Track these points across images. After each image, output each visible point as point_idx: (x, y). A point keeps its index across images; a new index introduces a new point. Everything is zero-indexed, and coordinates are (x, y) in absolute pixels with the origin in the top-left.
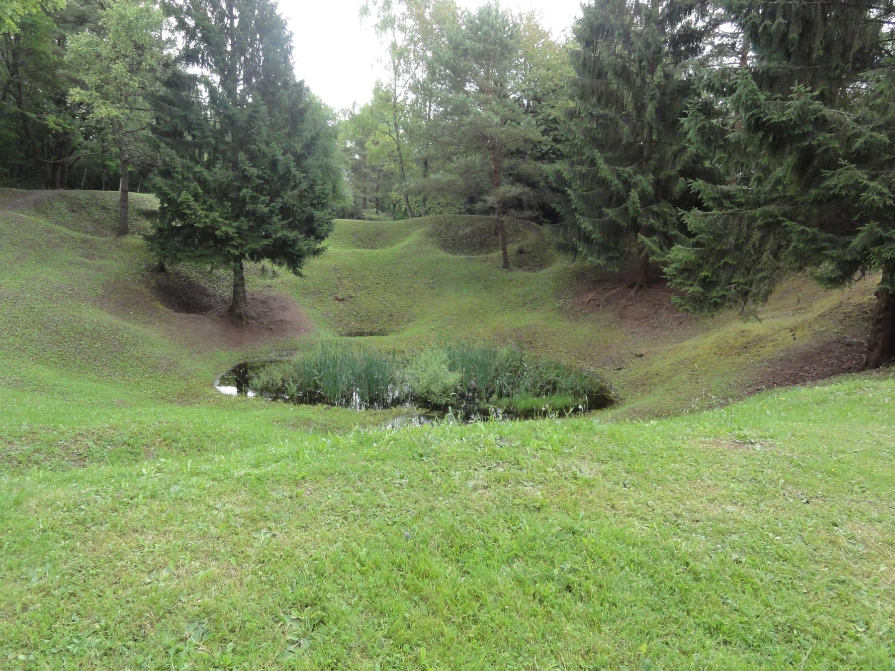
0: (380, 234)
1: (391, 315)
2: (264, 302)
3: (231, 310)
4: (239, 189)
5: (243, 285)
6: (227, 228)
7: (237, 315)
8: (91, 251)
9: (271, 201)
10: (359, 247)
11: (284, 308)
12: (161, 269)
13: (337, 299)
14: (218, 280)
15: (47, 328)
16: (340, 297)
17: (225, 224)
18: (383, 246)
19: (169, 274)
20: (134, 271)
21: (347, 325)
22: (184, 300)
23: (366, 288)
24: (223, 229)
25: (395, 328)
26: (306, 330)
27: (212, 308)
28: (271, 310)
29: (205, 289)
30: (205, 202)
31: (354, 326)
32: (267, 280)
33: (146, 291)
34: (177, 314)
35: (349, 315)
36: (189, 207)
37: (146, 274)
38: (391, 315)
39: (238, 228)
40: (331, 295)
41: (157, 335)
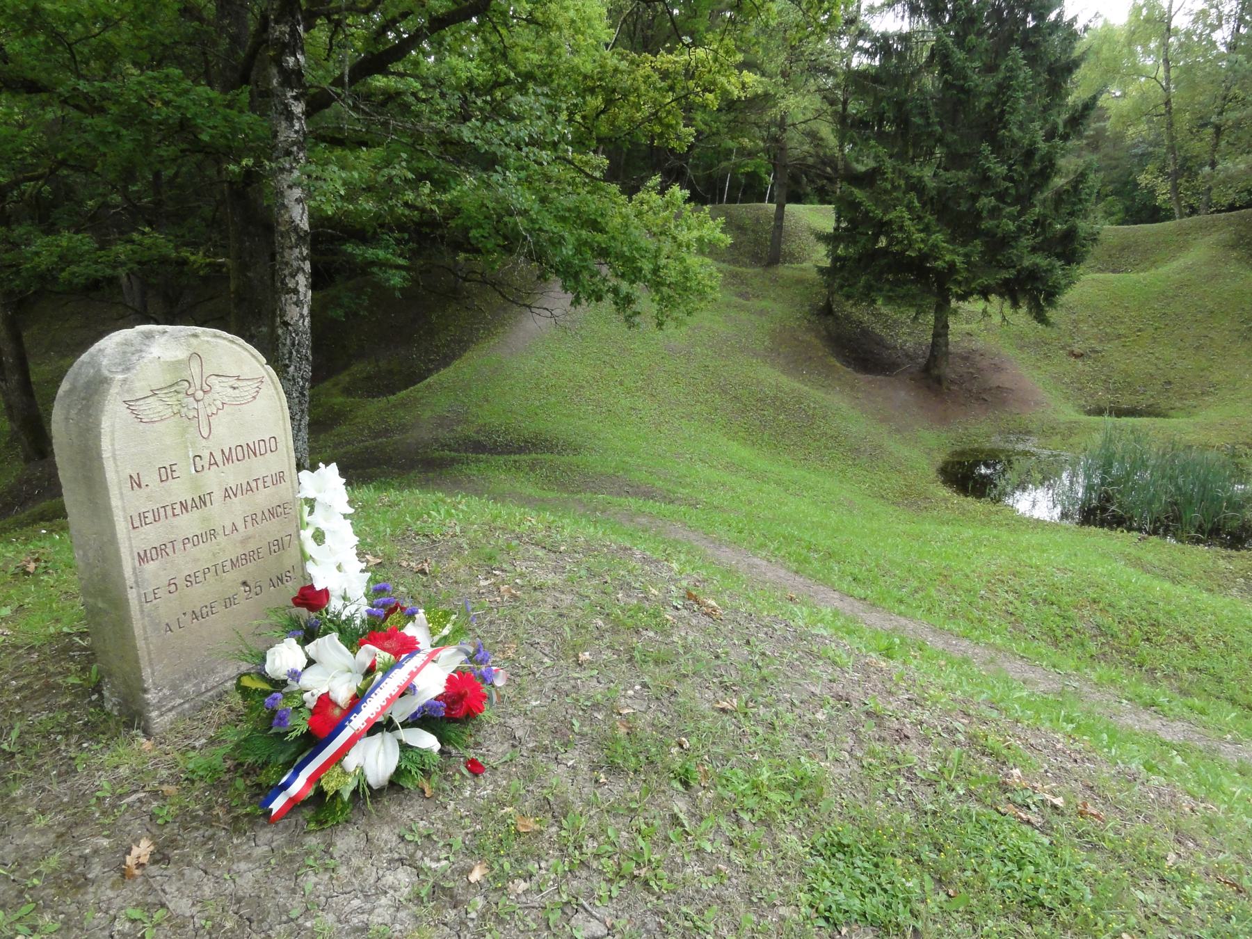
0: (1129, 247)
1: (1169, 383)
2: (966, 359)
3: (927, 369)
4: (974, 198)
5: (946, 335)
6: (952, 255)
7: (938, 378)
8: (743, 288)
9: (1021, 214)
10: (1100, 270)
11: (998, 368)
12: (827, 311)
13: (1072, 354)
14: (906, 328)
15: (726, 392)
16: (1077, 351)
17: (948, 251)
18: (1135, 266)
19: (837, 318)
20: (799, 315)
21: (1091, 396)
22: (863, 355)
23: (1119, 336)
24: (948, 258)
25: (1178, 404)
26: (1037, 404)
27: (898, 366)
28: (980, 370)
29: (882, 340)
30: (920, 218)
31: (1104, 398)
32: (983, 324)
33: (816, 342)
34: (860, 376)
35: (1094, 380)
36: (901, 228)
37: (813, 318)
38: (1169, 383)
39: (966, 255)
40: (1063, 348)
41: (845, 405)
